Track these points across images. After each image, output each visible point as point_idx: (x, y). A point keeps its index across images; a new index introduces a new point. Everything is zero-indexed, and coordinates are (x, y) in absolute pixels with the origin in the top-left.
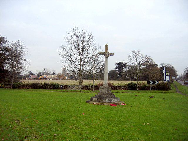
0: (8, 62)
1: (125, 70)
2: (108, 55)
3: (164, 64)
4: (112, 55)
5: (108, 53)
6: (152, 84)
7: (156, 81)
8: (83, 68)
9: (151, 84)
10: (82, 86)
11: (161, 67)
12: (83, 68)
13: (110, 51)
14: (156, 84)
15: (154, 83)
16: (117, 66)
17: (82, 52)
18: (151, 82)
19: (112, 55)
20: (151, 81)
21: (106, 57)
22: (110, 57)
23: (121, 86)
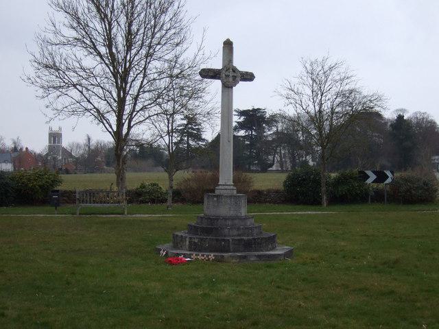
0: (62, 38)
1: (269, 132)
2: (234, 78)
3: (404, 110)
4: (248, 77)
5: (235, 70)
6: (375, 181)
7: (388, 173)
8: (130, 127)
9: (369, 181)
10: (128, 193)
11: (38, 145)
12: (130, 127)
13: (240, 64)
14: (389, 181)
15: (381, 177)
16: (242, 119)
17: (127, 72)
18: (373, 177)
19: (248, 77)
20: (369, 173)
21: (227, 88)
22: (240, 89)
23: (373, 201)
